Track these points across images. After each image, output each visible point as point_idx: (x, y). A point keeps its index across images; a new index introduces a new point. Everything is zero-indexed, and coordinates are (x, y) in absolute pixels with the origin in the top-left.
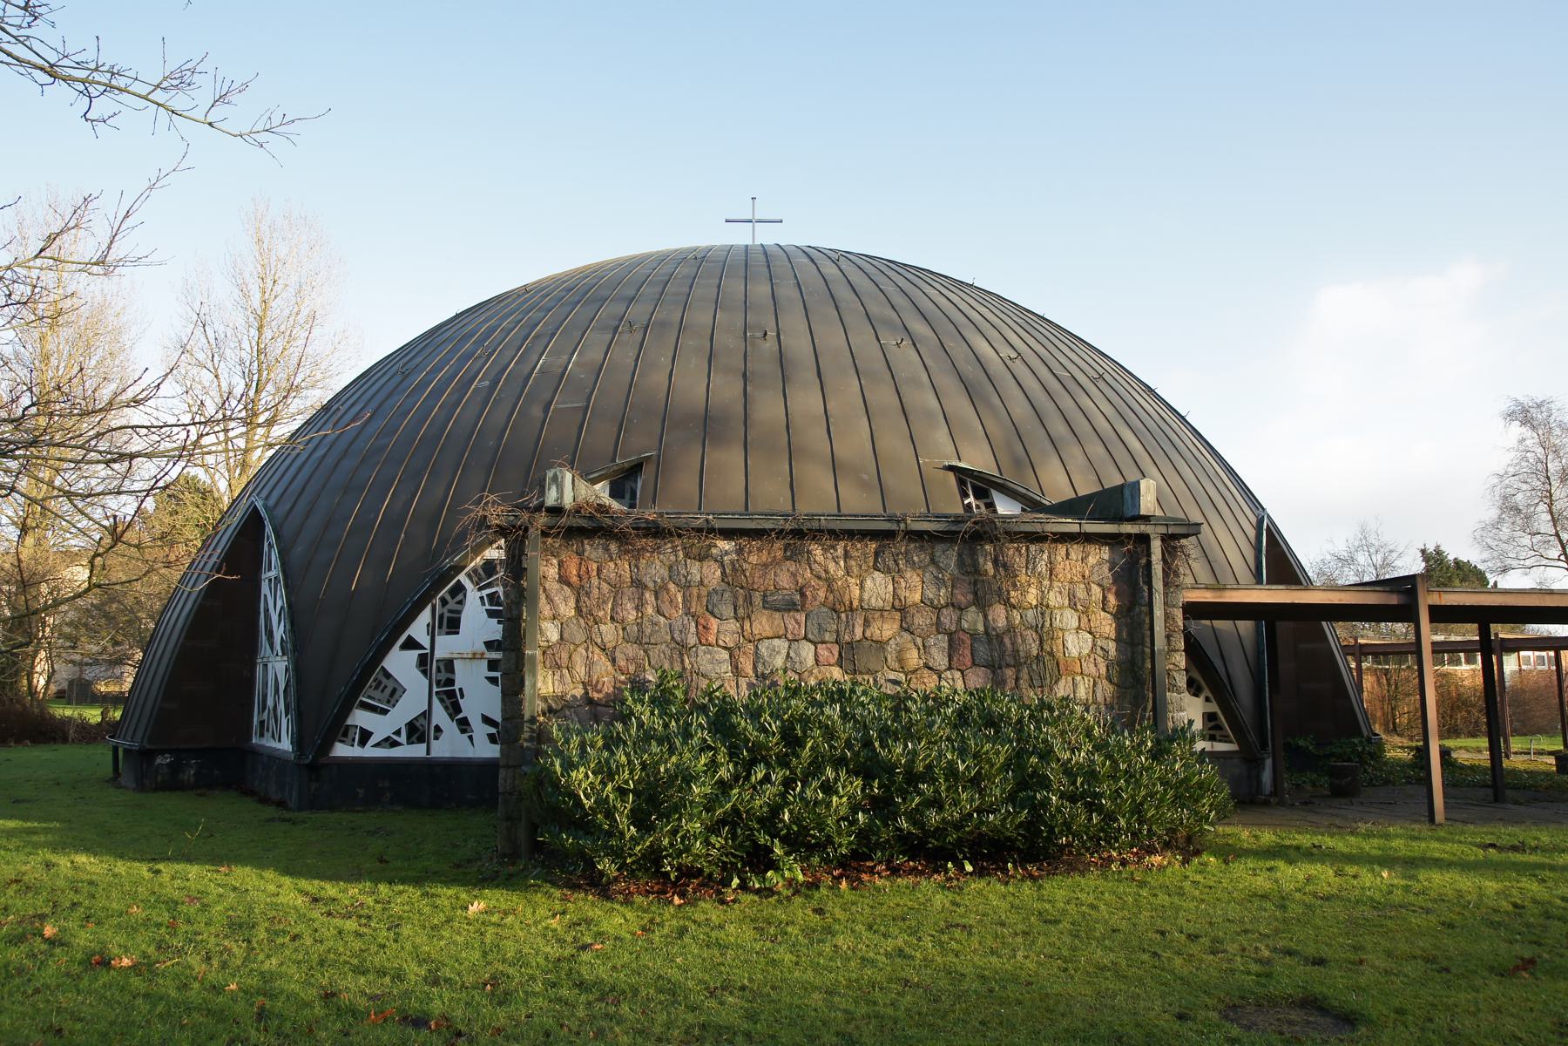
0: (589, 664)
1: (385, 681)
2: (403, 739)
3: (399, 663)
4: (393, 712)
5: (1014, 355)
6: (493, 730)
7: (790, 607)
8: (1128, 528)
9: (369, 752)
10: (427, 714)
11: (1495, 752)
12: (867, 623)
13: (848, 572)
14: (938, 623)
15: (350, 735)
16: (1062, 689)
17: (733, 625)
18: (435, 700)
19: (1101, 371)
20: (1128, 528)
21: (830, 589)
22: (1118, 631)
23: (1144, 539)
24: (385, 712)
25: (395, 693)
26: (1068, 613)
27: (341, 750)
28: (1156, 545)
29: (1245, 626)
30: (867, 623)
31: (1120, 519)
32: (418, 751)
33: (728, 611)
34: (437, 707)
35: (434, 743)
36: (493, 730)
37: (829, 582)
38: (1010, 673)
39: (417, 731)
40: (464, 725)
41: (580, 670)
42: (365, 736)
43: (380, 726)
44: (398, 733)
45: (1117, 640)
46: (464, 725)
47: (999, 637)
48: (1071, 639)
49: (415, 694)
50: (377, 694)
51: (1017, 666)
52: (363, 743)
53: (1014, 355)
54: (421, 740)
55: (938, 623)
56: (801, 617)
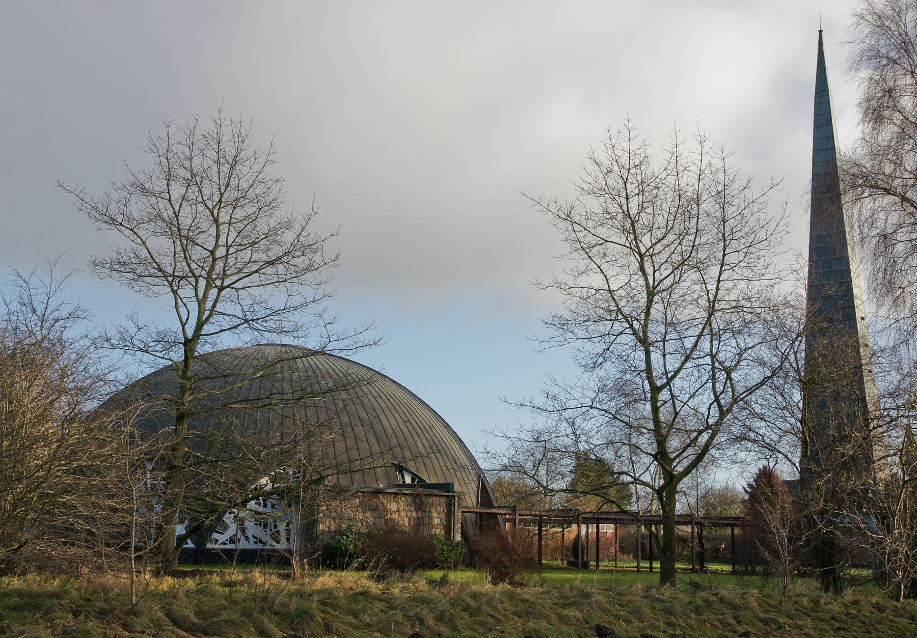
0: (330, 522)
1: (223, 524)
2: (228, 542)
3: (228, 518)
4: (225, 533)
5: (407, 420)
6: (256, 540)
7: (375, 510)
8: (450, 494)
9: (217, 546)
10: (235, 535)
11: (651, 565)
12: (391, 515)
13: (387, 502)
14: (407, 515)
15: (212, 541)
16: (433, 531)
17: (361, 514)
18: (239, 531)
19: (433, 424)
20: (450, 494)
21: (383, 506)
22: (446, 518)
23: (454, 497)
24: (223, 534)
25: (226, 528)
26: (435, 513)
27: (209, 546)
28: (457, 498)
29: (473, 515)
30: (391, 515)
31: (449, 492)
32: (232, 546)
33: (360, 510)
34: (239, 533)
35: (238, 544)
36: (256, 540)
37: (383, 504)
38: (422, 527)
39: (232, 540)
40: (247, 538)
41: (328, 524)
42: (217, 541)
43: (221, 538)
44: (227, 540)
45: (446, 521)
46: (247, 538)
47: (420, 519)
48: (435, 519)
49: (232, 529)
50: (220, 528)
51: (424, 526)
52: (216, 544)
53: (407, 420)
54: (233, 543)
55: (407, 515)
56: (377, 512)
